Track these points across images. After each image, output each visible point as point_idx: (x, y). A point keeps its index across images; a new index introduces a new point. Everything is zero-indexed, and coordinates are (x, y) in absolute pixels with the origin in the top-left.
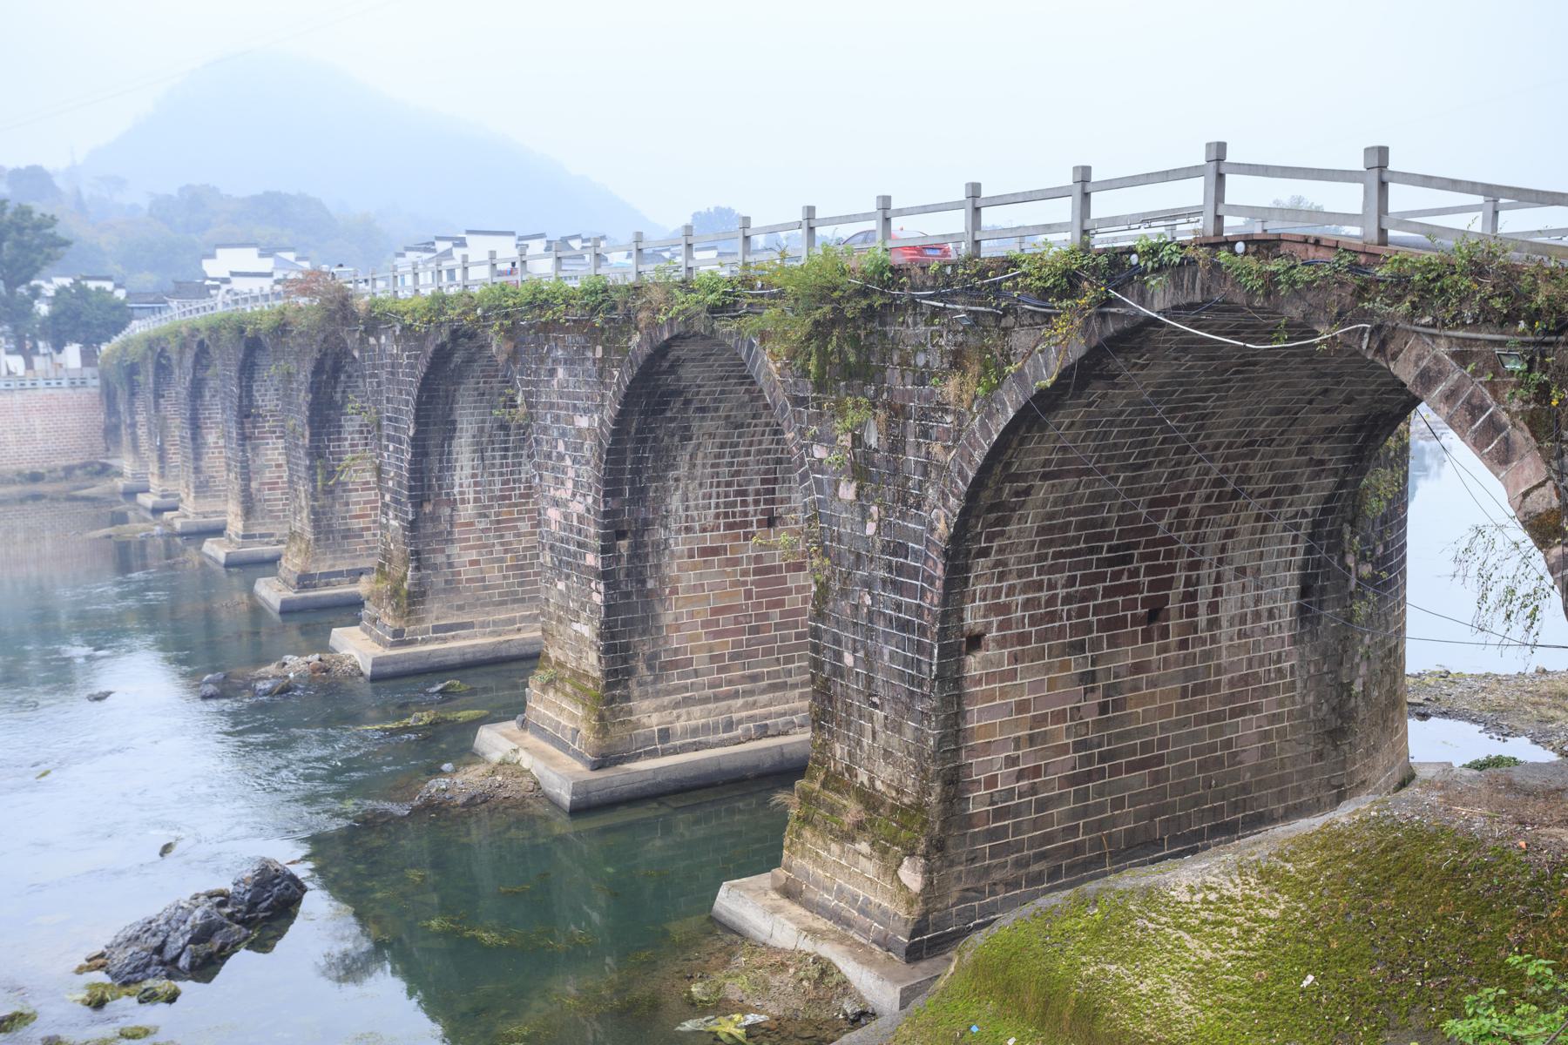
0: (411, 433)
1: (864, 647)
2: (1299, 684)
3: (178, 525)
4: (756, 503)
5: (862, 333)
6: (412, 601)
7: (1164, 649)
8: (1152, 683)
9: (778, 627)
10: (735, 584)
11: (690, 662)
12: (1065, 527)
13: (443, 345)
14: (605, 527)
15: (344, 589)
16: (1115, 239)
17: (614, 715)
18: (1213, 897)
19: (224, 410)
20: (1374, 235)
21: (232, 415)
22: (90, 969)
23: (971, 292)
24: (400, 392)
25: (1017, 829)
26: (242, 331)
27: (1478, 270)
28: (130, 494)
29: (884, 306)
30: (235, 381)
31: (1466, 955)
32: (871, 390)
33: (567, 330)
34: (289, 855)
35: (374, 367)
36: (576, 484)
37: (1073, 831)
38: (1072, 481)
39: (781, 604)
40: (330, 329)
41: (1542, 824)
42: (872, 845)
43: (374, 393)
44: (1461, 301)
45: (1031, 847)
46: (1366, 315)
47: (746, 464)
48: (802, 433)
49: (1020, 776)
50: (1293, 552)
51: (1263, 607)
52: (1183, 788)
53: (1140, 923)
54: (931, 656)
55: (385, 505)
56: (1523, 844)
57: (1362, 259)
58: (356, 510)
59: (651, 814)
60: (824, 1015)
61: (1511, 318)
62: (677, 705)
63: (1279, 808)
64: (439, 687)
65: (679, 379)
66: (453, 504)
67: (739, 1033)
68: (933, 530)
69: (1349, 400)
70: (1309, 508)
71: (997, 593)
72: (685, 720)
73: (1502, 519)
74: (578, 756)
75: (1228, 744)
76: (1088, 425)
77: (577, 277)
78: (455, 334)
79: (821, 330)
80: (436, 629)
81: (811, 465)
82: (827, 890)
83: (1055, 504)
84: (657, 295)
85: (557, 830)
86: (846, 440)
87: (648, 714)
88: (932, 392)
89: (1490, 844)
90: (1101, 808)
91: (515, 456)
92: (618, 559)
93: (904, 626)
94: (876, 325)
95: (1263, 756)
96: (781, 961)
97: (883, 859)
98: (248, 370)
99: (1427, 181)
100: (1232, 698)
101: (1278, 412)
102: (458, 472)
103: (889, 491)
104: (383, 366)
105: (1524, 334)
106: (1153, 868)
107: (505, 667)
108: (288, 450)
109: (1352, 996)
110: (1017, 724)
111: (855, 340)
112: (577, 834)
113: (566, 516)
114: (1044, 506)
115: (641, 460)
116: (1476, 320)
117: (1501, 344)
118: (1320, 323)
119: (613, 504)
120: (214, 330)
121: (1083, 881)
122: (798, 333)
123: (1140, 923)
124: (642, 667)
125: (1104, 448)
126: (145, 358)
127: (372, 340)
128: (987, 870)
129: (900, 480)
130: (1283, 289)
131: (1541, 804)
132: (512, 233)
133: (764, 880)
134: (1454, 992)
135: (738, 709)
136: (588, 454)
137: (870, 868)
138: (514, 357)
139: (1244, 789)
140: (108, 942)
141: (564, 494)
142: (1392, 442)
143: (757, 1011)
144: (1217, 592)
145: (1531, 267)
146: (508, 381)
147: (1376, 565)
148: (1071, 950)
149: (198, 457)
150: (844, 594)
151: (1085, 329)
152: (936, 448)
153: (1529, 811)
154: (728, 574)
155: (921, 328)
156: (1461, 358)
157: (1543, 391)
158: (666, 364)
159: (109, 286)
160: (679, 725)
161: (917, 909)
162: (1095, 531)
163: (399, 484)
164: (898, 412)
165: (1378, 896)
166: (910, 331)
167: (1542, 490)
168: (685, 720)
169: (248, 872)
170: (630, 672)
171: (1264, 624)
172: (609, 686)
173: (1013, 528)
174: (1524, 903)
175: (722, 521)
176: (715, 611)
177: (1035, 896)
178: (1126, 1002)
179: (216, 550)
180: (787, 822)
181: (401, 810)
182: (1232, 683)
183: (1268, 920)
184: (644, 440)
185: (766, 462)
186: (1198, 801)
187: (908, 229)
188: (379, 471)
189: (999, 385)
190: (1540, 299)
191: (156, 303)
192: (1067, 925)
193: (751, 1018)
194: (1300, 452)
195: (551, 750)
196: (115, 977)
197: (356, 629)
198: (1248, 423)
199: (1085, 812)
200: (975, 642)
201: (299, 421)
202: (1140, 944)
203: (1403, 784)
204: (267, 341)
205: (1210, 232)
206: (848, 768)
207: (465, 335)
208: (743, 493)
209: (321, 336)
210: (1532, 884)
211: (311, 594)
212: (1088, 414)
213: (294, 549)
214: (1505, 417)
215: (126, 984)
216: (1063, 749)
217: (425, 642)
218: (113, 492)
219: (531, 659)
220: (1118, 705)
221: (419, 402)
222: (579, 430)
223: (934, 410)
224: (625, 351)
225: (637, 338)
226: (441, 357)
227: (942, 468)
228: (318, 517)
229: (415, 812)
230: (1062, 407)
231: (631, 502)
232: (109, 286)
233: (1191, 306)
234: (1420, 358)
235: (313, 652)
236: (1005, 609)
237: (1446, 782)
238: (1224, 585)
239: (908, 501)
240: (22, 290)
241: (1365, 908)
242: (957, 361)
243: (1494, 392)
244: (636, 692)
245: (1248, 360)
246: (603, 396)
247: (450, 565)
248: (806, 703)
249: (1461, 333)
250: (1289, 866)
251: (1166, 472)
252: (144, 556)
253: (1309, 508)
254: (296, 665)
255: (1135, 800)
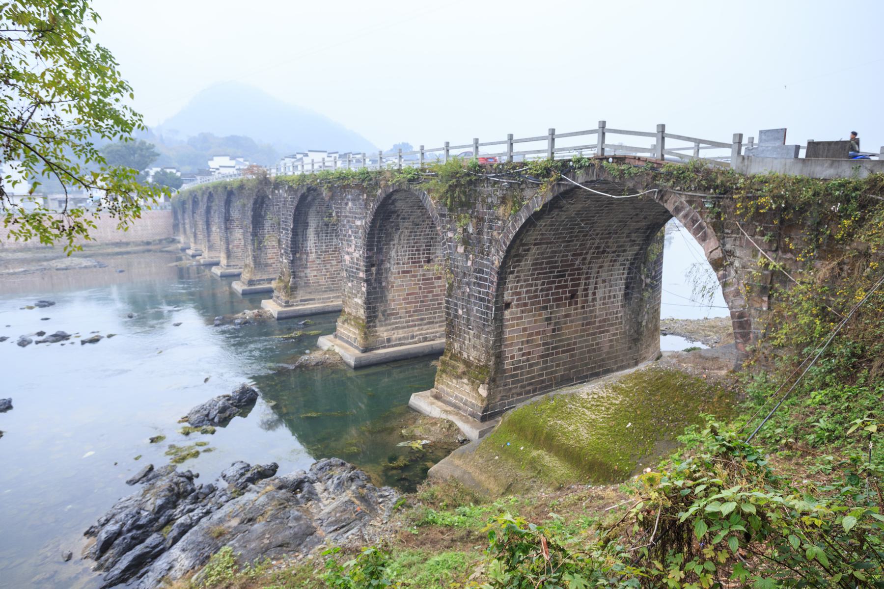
0: (292, 227)
1: (466, 307)
2: (624, 322)
3: (202, 261)
4: (423, 254)
5: (467, 190)
6: (292, 290)
7: (576, 309)
8: (572, 321)
9: (431, 300)
10: (415, 284)
11: (398, 313)
12: (542, 263)
13: (304, 193)
14: (367, 262)
15: (266, 286)
16: (564, 156)
17: (370, 333)
18: (596, 396)
19: (219, 218)
20: (660, 157)
21: (222, 220)
22: (183, 422)
23: (509, 175)
24: (287, 211)
25: (522, 374)
26: (226, 188)
27: (697, 170)
28: (183, 250)
29: (476, 180)
30: (223, 207)
31: (684, 415)
32: (470, 211)
33: (353, 188)
34: (250, 383)
35: (277, 202)
36: (356, 246)
37: (542, 375)
38: (544, 246)
39: (432, 292)
40: (260, 187)
41: (711, 369)
42: (469, 380)
43: (277, 211)
44: (691, 181)
45: (526, 381)
46: (656, 186)
47: (420, 239)
48: (443, 227)
49: (523, 355)
50: (623, 274)
51: (612, 294)
52: (581, 360)
53: (569, 406)
54: (492, 311)
55: (282, 254)
56: (705, 376)
57: (655, 165)
58: (269, 256)
59: (384, 369)
60: (451, 441)
61: (708, 188)
62: (393, 329)
63: (615, 367)
64: (303, 322)
65: (395, 207)
66: (307, 254)
67: (420, 447)
68: (493, 264)
69: (645, 218)
70: (629, 258)
71: (516, 287)
72: (396, 335)
73: (701, 261)
74: (356, 348)
75: (598, 344)
76: (551, 225)
77: (354, 168)
78: (309, 189)
79: (452, 188)
80: (301, 301)
81: (447, 239)
82: (452, 396)
83: (538, 255)
84: (388, 175)
85: (349, 375)
86: (460, 230)
87: (383, 332)
88: (494, 213)
89: (694, 376)
90: (552, 367)
91: (331, 236)
92: (372, 274)
93: (482, 299)
94: (472, 187)
95: (610, 348)
96: (435, 422)
97: (472, 385)
98: (228, 203)
99: (679, 137)
100: (600, 327)
101: (620, 222)
102: (309, 242)
103: (477, 249)
104: (280, 202)
105: (712, 194)
106: (574, 387)
107: (327, 315)
108: (244, 234)
109: (644, 430)
110: (522, 336)
111: (464, 193)
112: (356, 377)
113: (352, 258)
114: (534, 255)
115: (380, 237)
116: (695, 189)
117: (704, 197)
118: (640, 189)
119: (370, 254)
120: (215, 187)
121: (548, 392)
122: (443, 190)
123: (569, 406)
124: (380, 315)
125: (557, 234)
126: (188, 198)
127: (276, 192)
128: (510, 389)
129: (481, 245)
130: (626, 176)
131: (711, 363)
132: (326, 152)
133: (428, 393)
134: (679, 427)
135: (416, 331)
136: (360, 235)
137: (468, 388)
138: (332, 198)
139: (603, 360)
140: (188, 412)
141: (351, 250)
142: (659, 234)
143: (426, 439)
144: (596, 288)
145: (716, 170)
146: (328, 207)
147: (652, 279)
148: (544, 416)
149: (209, 236)
150: (459, 288)
151: (552, 190)
152: (495, 233)
153: (707, 365)
154: (413, 281)
155: (490, 188)
156: (690, 202)
157: (718, 215)
158: (391, 201)
159: (174, 171)
160: (394, 337)
161: (485, 403)
162: (552, 264)
163: (287, 246)
164: (481, 220)
165: (655, 395)
166: (486, 189)
167: (717, 251)
168: (396, 335)
169: (238, 388)
170: (376, 317)
171: (612, 300)
172: (368, 322)
173: (523, 263)
174: (704, 396)
175: (410, 261)
176: (408, 294)
177: (527, 398)
178: (564, 433)
179: (217, 271)
180: (436, 372)
181: (292, 367)
182: (600, 321)
183: (615, 404)
184: (382, 230)
185: (427, 239)
186: (587, 364)
187: (484, 151)
188: (279, 241)
189: (519, 210)
190: (719, 181)
191: (192, 177)
192: (543, 407)
193: (424, 442)
194: (627, 237)
195: (347, 345)
196: (192, 424)
197: (271, 301)
198: (609, 226)
199: (546, 368)
200: (508, 305)
201: (248, 222)
202: (569, 413)
203: (658, 359)
204: (235, 192)
205: (600, 154)
206: (460, 352)
207: (313, 190)
208: (418, 250)
209: (257, 190)
210: (707, 390)
211: (253, 287)
212: (552, 221)
213: (246, 270)
214: (705, 224)
215: (196, 427)
216: (539, 345)
217: (297, 305)
218: (177, 250)
219: (338, 312)
220: (559, 330)
221: (295, 215)
222: (357, 226)
223: (495, 219)
224: (375, 196)
225: (380, 191)
226: (303, 198)
227: (497, 241)
228: (256, 259)
229: (296, 367)
230: (542, 218)
231: (377, 253)
232: (174, 171)
233: (592, 182)
234: (675, 202)
235: (255, 309)
236: (519, 293)
237: (676, 355)
238: (598, 286)
239: (483, 253)
240: (142, 173)
241: (650, 399)
242: (503, 200)
243: (701, 215)
244: (378, 324)
245: (610, 201)
246: (366, 213)
247: (306, 277)
248: (444, 329)
249: (690, 193)
250: (623, 385)
251: (579, 243)
252: (189, 273)
253: (629, 258)
254: (249, 314)
255: (564, 364)
